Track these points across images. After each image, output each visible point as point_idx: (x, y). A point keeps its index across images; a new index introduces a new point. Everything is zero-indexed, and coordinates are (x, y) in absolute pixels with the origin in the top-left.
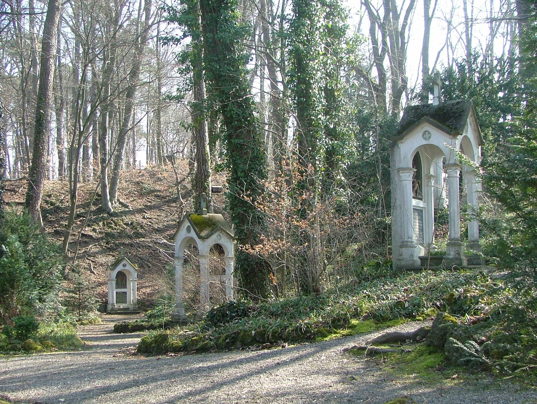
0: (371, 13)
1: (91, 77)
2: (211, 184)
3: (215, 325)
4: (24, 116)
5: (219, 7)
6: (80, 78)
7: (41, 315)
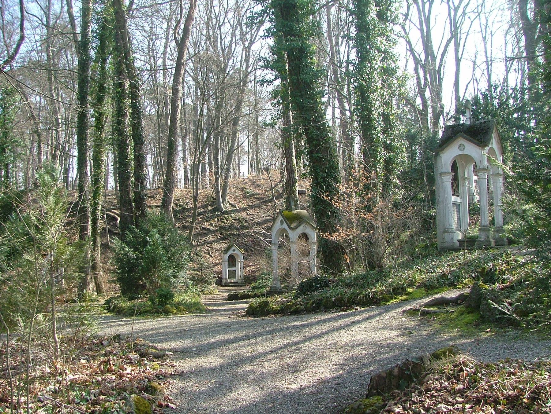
0: (415, 58)
1: (206, 112)
2: (298, 188)
3: (304, 293)
4: (159, 142)
5: (301, 56)
6: (199, 113)
7: (175, 287)
